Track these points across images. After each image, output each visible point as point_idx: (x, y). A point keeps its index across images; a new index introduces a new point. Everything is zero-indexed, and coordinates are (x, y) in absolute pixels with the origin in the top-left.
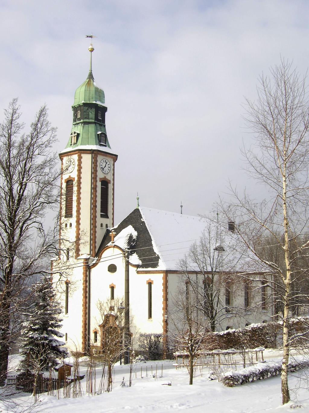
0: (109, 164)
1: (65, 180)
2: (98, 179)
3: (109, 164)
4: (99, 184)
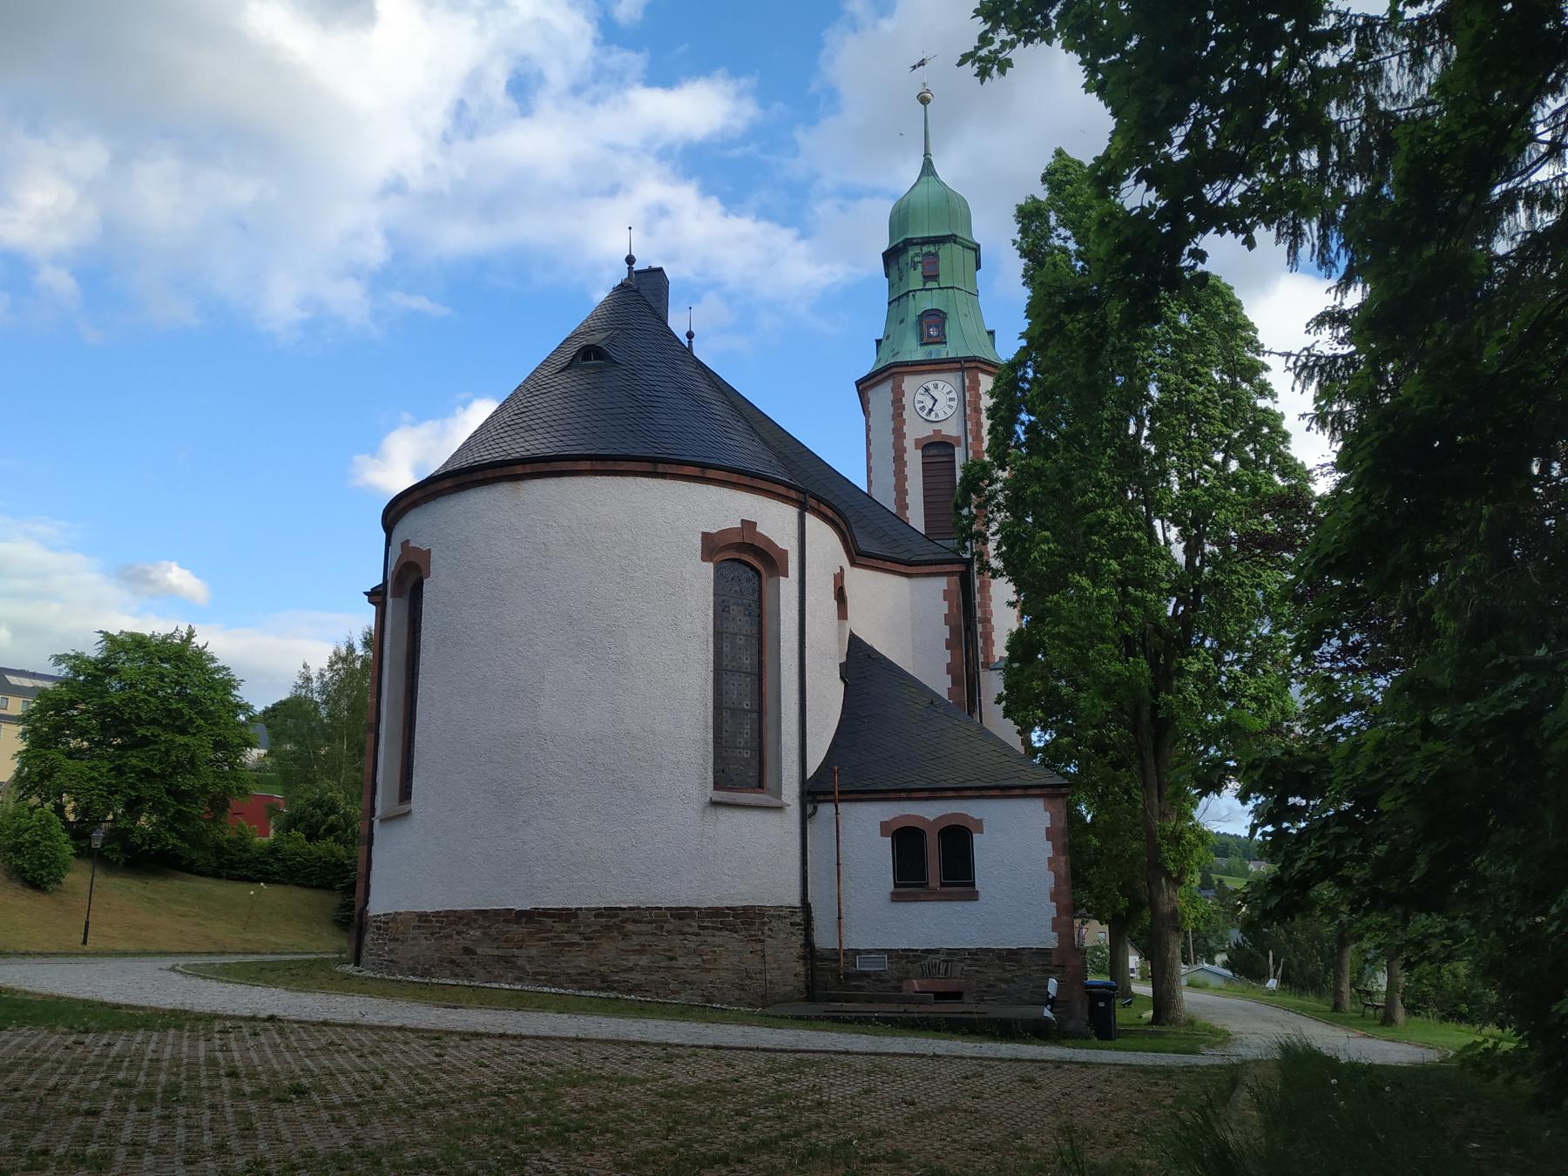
0: (951, 392)
1: (917, 441)
2: (909, 443)
3: (951, 392)
4: (914, 459)
